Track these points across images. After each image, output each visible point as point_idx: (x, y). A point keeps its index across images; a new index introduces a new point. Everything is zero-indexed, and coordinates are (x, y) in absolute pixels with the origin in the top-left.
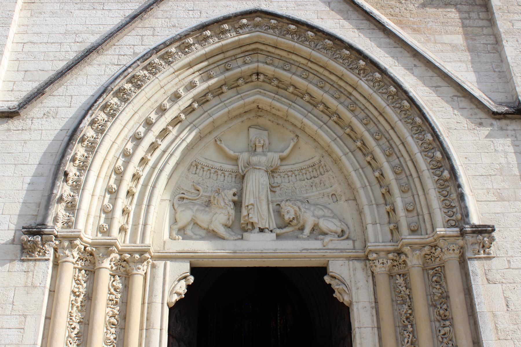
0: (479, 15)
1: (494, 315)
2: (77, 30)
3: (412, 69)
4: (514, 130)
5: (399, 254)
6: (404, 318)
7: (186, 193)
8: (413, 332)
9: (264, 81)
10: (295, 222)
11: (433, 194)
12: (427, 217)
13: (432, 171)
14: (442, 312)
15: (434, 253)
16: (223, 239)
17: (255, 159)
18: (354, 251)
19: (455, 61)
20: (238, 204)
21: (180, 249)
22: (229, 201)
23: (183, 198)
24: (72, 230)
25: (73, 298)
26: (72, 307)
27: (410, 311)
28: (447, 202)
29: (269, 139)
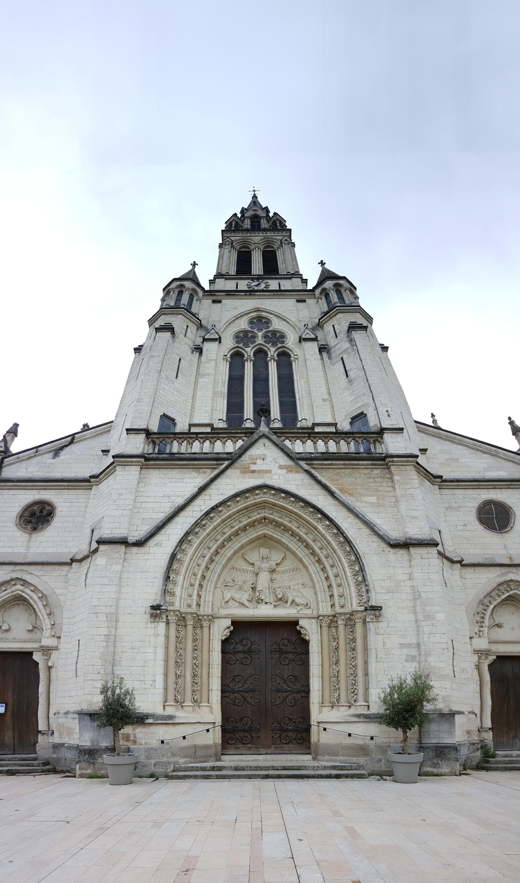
0: (387, 484)
1: (377, 651)
5: (334, 617)
6: (334, 648)
9: (268, 523)
10: (283, 599)
11: (353, 589)
12: (349, 600)
14: (352, 647)
16: (248, 607)
17: (263, 565)
19: (371, 513)
20: (254, 589)
21: (226, 613)
22: (249, 588)
23: (227, 586)
25: (176, 639)
27: (337, 646)
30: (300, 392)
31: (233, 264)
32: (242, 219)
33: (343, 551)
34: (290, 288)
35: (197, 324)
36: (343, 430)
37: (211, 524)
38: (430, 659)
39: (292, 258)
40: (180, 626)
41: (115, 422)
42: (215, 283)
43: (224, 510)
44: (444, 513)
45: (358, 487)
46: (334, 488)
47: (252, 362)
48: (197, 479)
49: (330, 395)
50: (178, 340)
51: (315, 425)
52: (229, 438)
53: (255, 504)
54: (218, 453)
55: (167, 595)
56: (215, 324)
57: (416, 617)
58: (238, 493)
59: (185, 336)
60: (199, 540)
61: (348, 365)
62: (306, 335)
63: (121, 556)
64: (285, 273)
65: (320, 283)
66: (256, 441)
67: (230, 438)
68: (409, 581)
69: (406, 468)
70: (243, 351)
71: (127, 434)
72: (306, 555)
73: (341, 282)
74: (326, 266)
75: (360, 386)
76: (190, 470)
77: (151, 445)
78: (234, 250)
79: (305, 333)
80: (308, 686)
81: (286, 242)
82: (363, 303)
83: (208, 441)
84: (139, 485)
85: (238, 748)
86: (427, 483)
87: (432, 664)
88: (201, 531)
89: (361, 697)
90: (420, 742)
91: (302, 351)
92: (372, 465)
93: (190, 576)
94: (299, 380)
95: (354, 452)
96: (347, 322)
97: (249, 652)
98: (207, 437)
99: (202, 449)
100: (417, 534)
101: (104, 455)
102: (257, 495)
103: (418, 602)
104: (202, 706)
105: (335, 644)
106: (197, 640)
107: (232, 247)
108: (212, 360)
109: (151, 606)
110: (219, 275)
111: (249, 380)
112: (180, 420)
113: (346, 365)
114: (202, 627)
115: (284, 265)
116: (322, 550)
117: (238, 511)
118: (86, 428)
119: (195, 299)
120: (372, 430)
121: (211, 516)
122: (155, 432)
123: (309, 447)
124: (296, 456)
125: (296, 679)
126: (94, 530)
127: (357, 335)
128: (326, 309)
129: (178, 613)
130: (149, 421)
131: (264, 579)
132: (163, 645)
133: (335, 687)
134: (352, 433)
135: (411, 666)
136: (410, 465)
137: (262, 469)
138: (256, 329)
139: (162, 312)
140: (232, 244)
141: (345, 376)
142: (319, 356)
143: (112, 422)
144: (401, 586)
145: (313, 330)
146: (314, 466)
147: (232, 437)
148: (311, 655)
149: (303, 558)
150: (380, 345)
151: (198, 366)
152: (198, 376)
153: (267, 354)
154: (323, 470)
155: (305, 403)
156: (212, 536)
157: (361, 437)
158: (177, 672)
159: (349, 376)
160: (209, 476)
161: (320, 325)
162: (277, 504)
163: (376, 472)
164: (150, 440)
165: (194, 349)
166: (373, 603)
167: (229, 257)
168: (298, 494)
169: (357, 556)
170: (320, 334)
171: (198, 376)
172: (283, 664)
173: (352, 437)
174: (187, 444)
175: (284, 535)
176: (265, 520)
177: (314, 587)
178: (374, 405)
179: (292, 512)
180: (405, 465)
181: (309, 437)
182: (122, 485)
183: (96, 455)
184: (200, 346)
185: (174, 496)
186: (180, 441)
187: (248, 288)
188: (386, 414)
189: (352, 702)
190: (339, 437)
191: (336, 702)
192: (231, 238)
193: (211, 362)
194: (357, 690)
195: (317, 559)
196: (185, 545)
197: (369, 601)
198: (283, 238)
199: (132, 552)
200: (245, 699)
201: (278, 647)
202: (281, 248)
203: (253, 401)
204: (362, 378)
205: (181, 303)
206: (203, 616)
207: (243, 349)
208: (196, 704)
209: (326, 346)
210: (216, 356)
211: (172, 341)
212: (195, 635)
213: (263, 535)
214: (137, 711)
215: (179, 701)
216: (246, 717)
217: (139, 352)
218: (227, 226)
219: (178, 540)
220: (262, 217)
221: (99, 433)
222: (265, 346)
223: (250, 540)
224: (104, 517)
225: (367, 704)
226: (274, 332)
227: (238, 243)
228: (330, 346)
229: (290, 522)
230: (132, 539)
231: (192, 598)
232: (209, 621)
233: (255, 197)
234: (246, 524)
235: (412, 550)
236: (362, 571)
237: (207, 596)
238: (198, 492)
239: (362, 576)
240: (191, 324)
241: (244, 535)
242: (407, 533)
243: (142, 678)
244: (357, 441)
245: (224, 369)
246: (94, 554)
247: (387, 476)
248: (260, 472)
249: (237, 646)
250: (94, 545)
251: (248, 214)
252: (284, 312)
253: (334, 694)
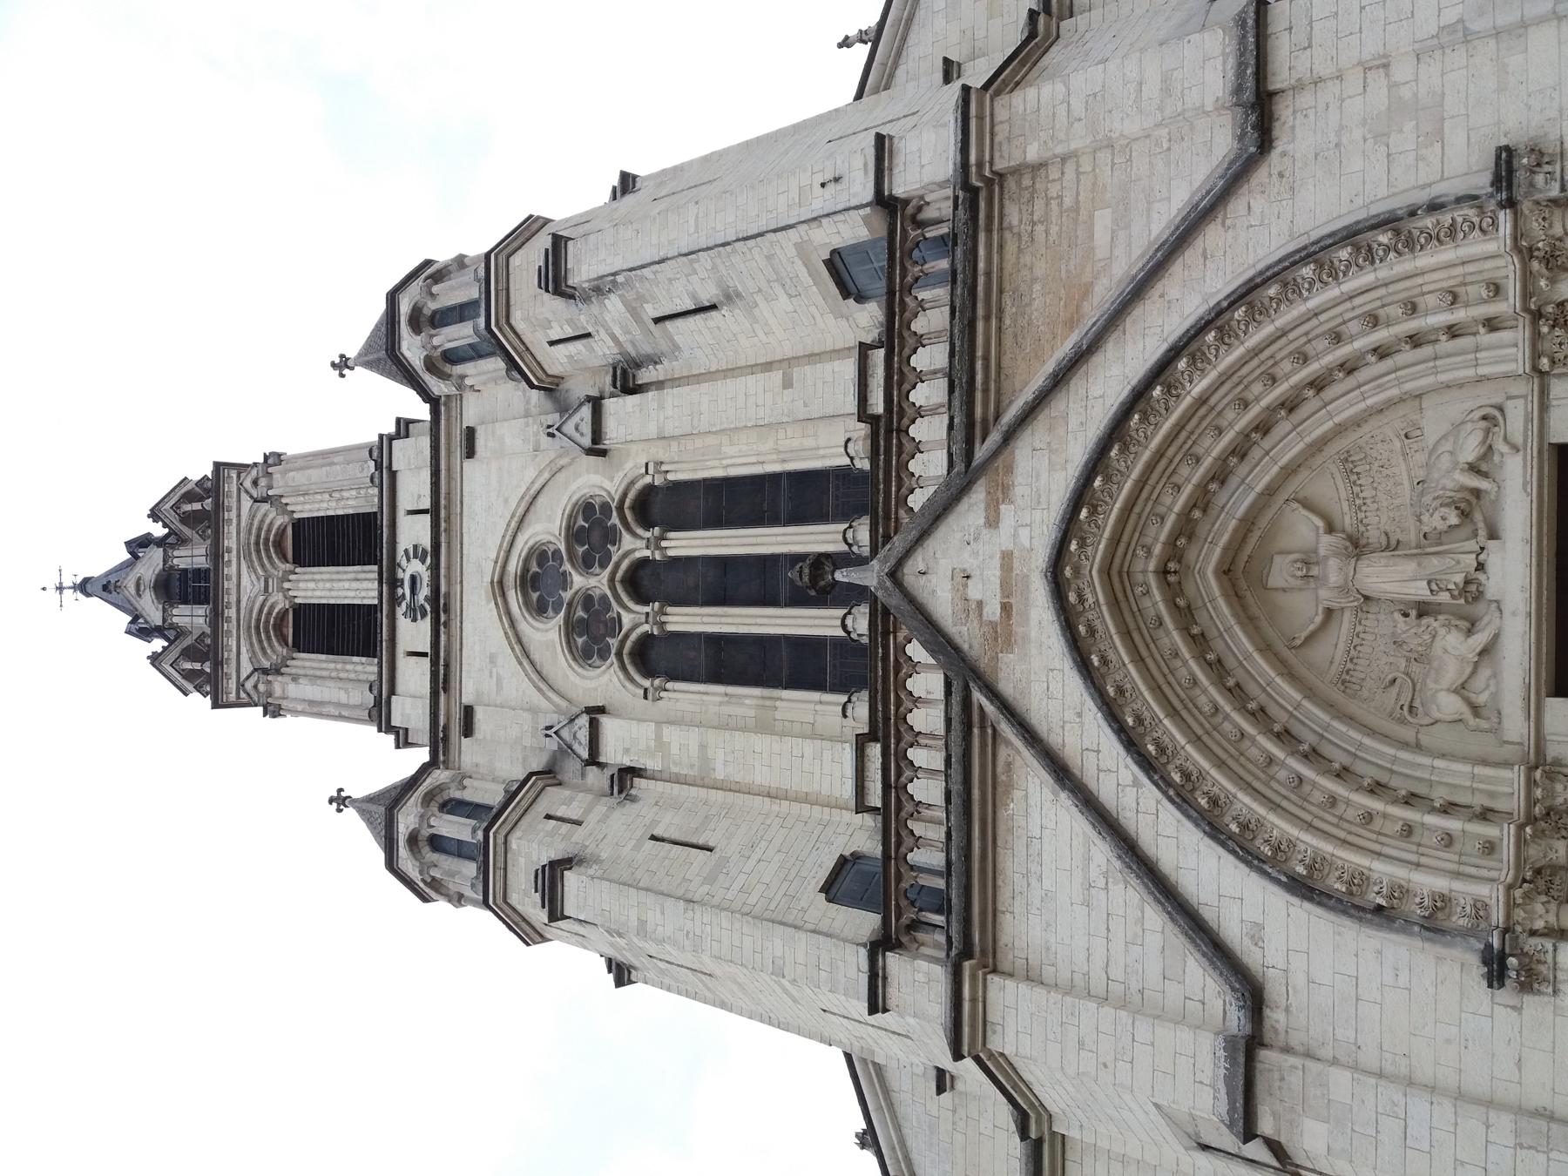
0: (1054, 180)
2: (1082, 884)
3: (1169, 302)
7: (1401, 703)
10: (1463, 505)
12: (1470, 268)
13: (1378, 262)
15: (1546, 253)
17: (1334, 578)
18: (1530, 398)
22: (1419, 626)
23: (1411, 707)
24: (1494, 902)
28: (1442, 234)
29: (1289, 553)
30: (761, 459)
31: (339, 666)
32: (171, 634)
34: (426, 475)
35: (540, 784)
39: (323, 466)
42: (407, 730)
43: (1135, 707)
45: (1063, 272)
47: (669, 609)
48: (1030, 791)
49: (771, 363)
50: (592, 846)
51: (863, 414)
53: (1114, 603)
54: (948, 721)
55: (1446, 925)
56: (542, 726)
57: (1541, 20)
58: (1075, 661)
59: (578, 823)
60: (1240, 795)
61: (678, 301)
62: (582, 434)
63: (1296, 1068)
64: (376, 491)
65: (408, 376)
66: (911, 600)
67: (900, 683)
68: (1393, 69)
69: (1002, 122)
70: (633, 637)
71: (885, 1010)
72: (1295, 428)
73: (405, 308)
74: (352, 353)
75: (745, 268)
76: (1002, 814)
77: (920, 936)
78: (289, 663)
79: (577, 436)
81: (263, 482)
82: (478, 243)
83: (911, 753)
86: (1054, 56)
91: (634, 447)
92: (989, 230)
94: (725, 462)
95: (949, 287)
96: (540, 297)
99: (932, 772)
100: (1224, 71)
101: (952, 1087)
102: (1081, 599)
107: (278, 672)
108: (659, 736)
109: (1490, 986)
110: (380, 715)
111: (724, 620)
112: (845, 838)
113: (679, 309)
115: (345, 494)
117: (1139, 660)
118: (868, 1139)
119: (457, 795)
121: (1154, 753)
123: (930, 431)
127: (582, 270)
128: (497, 364)
129: (1518, 893)
130: (845, 940)
131: (1384, 577)
134: (891, 293)
138: (563, 594)
139: (500, 901)
140: (265, 672)
141: (714, 313)
142: (650, 394)
143: (848, 1057)
144: (1416, 95)
145: (567, 411)
146: (991, 419)
150: (614, 198)
151: (678, 780)
152: (706, 780)
153: (644, 562)
154: (1006, 385)
155: (795, 443)
156: (1225, 750)
159: (715, 300)
160: (1018, 752)
161: (551, 387)
163: (1013, 215)
164: (904, 939)
165: (623, 795)
167: (314, 679)
168: (1083, 463)
169: (1302, 259)
170: (580, 388)
171: (706, 780)
173: (901, 295)
174: (918, 820)
175: (1223, 508)
177: (1419, 396)
178: (805, 226)
180: (992, 126)
182: (1051, 1037)
183: (954, 1111)
184: (612, 776)
185: (1086, 869)
186: (908, 841)
187: (424, 615)
188: (831, 187)
190: (901, 337)
192: (244, 675)
193: (665, 739)
195: (1311, 393)
196: (1258, 842)
197: (1475, 198)
198: (247, 492)
199: (1281, 1027)
202: (284, 501)
204: (718, 261)
205: (469, 839)
206: (1531, 802)
207: (627, 636)
209: (619, 372)
210: (645, 724)
211: (595, 867)
217: (630, 968)
218: (198, 688)
219: (1242, 866)
220: (165, 562)
221: (885, 1100)
222: (617, 565)
223: (1240, 623)
226: (574, 535)
227: (263, 649)
228: (619, 357)
232: (1552, 780)
233: (84, 587)
234: (1182, 636)
237: (1453, 777)
238: (1072, 791)
239: (1375, 232)
240: (542, 807)
242: (1220, 102)
244: (917, 280)
245: (688, 697)
247: (1026, 182)
248: (1006, 587)
251: (153, 613)
252: (506, 501)
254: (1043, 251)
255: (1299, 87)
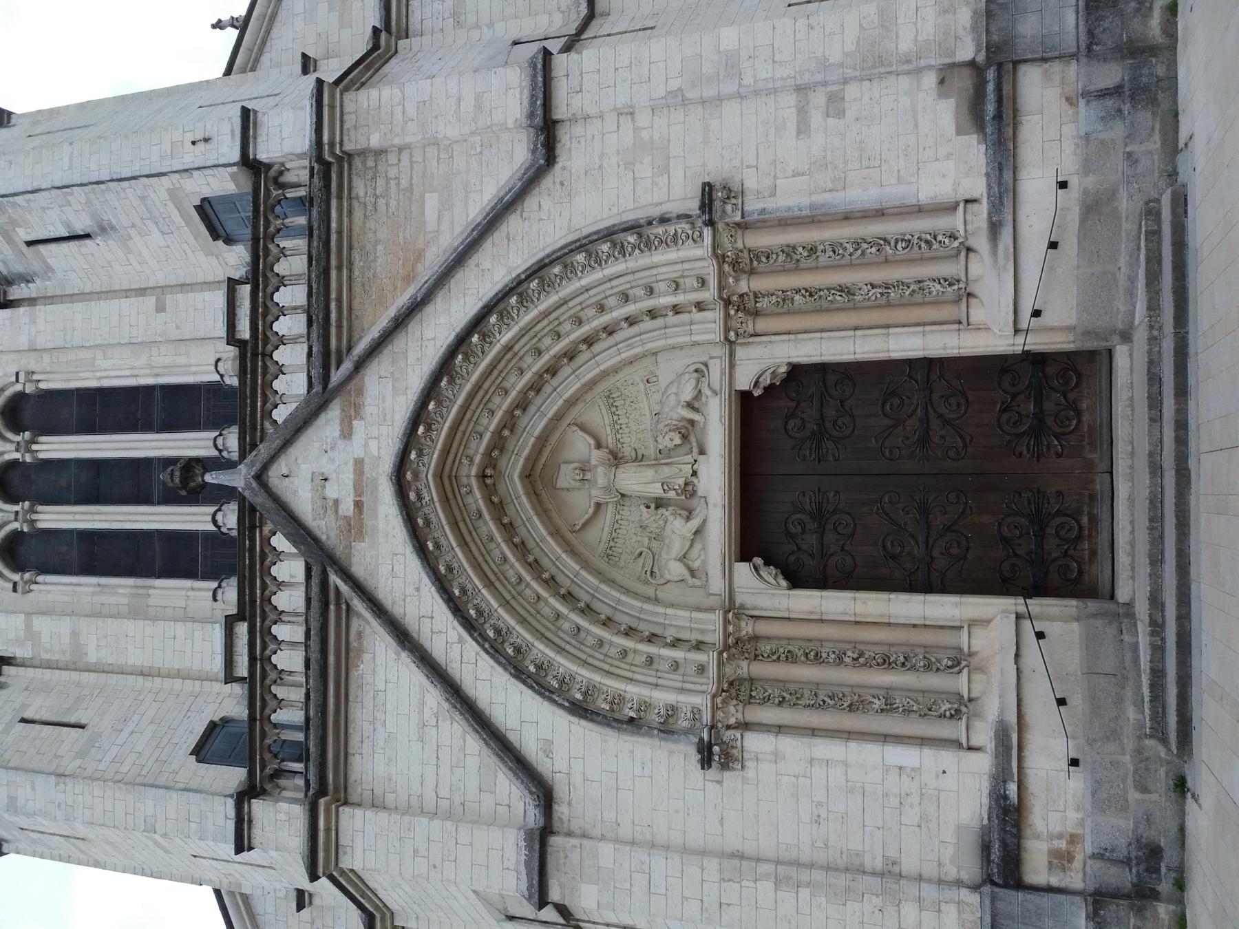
0: (392, 165)
3: (483, 271)
4: (571, 138)
5: (730, 303)
8: (828, 289)
10: (683, 431)
11: (659, 257)
12: (686, 266)
14: (805, 254)
16: (705, 521)
17: (601, 481)
23: (652, 572)
26: (798, 704)
27: (803, 292)
28: (669, 240)
33: (564, 282)
36: (248, 264)
37: (495, 614)
38: (835, 56)
40: (753, 694)
41: (217, 882)
43: (461, 581)
44: (469, 29)
45: (401, 237)
46: (403, 299)
47: (40, 508)
48: (377, 654)
51: (232, 338)
52: (266, 571)
53: (445, 500)
54: (308, 600)
57: (730, 97)
58: (414, 546)
60: (537, 644)
63: (575, 847)
69: (349, 113)
71: (250, 848)
72: (573, 372)
76: (354, 674)
77: (282, 782)
80: (910, 362)
83: (275, 630)
84: (393, 806)
85: (1093, 553)
86: (393, 66)
87: (850, 47)
88: (512, 641)
89: (941, 223)
90: (1074, 56)
92: (340, 198)
93: (628, 667)
97: (819, 515)
98: (261, 631)
99: (293, 644)
100: (521, 99)
101: (311, 903)
102: (420, 497)
103: (690, 95)
104: (969, 648)
105: (797, 297)
106: (789, 652)
108: (29, 627)
109: (703, 768)
111: (96, 517)
114: (756, 638)
116: (562, 333)
117: (464, 544)
120: (248, 188)
121: (474, 616)
122: (246, 775)
124: (317, 393)
125: (892, 394)
126: (509, 914)
129: (719, 700)
130: (214, 794)
132: (806, 740)
133: (914, 291)
134: (255, 240)
135: (855, 100)
136: (342, 99)
137: (352, 484)
143: (218, 893)
144: (651, 138)
147: (262, 563)
148: (827, 358)
149: (583, 381)
151: (49, 665)
154: (356, 323)
157: (267, 220)
158: (876, 707)
160: (368, 623)
162: (444, 445)
163: (360, 188)
164: (268, 787)
166: (693, 206)
168: (419, 391)
172: (853, 431)
174: (282, 685)
176: (486, 476)
177: (655, 354)
178: (177, 175)
179: (465, 408)
181: (264, 355)
185: (421, 712)
186: (272, 704)
188: (201, 146)
189: (956, 244)
190: (265, 276)
191: (955, 287)
193: (35, 629)
194: (923, 236)
196: (549, 678)
197: (689, 216)
199: (565, 818)
200: (948, 529)
201: (808, 444)
203: (160, 503)
206: (727, 635)
208: (964, 663)
212: (775, 657)
213: (526, 480)
214: (985, 822)
215: (956, 706)
216: (999, 530)
219: (538, 697)
223: (537, 514)
224: (474, 891)
225: (962, 205)
229: (492, 412)
230: (533, 817)
231: (681, 661)
235: (560, 112)
236: (614, 233)
239: (625, 234)
241: (524, 529)
242: (519, 123)
243: (894, 802)
244: (279, 231)
246: (572, 915)
248: (359, 487)
249: (804, 547)
250: (549, 914)
253: (934, 293)
254: (384, 219)
255: (573, 120)
